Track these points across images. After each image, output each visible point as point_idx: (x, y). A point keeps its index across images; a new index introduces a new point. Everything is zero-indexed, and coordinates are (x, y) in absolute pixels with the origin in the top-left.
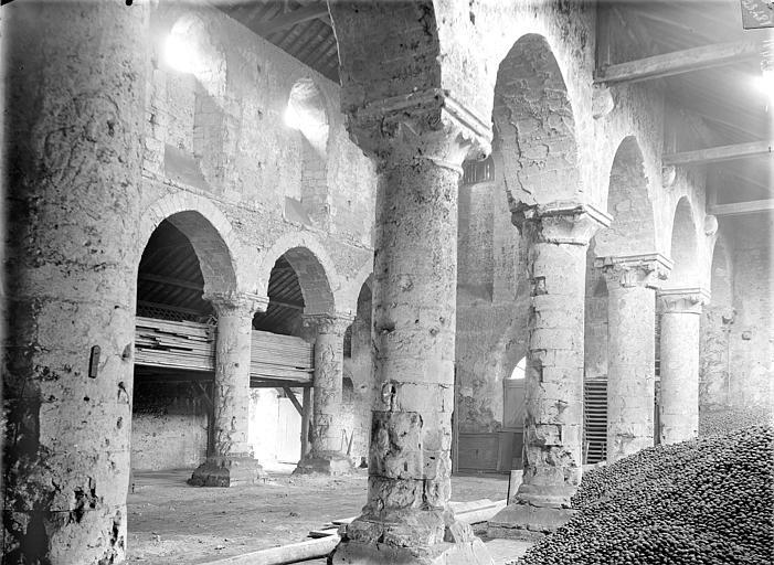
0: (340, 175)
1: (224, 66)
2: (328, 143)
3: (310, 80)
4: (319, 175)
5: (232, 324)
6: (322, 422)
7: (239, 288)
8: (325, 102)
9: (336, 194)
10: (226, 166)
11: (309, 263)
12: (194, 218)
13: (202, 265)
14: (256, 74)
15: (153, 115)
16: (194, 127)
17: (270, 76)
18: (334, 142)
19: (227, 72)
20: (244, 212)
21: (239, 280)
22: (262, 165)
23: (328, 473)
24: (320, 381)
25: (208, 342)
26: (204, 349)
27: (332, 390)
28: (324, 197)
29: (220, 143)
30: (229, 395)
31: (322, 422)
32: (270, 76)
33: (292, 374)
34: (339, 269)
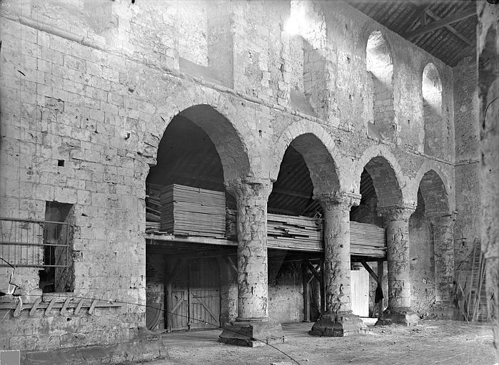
0: (402, 101)
1: (324, 26)
2: (393, 78)
3: (379, 32)
4: (387, 102)
5: (337, 216)
6: (396, 286)
7: (342, 188)
8: (390, 48)
9: (400, 116)
10: (329, 99)
11: (384, 168)
12: (310, 136)
13: (311, 175)
14: (345, 30)
15: (282, 65)
16: (304, 74)
17: (354, 31)
18: (397, 77)
19: (326, 29)
20: (342, 133)
21: (341, 182)
22: (352, 98)
23: (405, 324)
24: (394, 256)
25: (317, 231)
26: (315, 236)
27: (403, 262)
28: (392, 118)
29: (324, 83)
30: (337, 268)
31: (396, 286)
32: (354, 31)
33: (373, 252)
34: (404, 171)
